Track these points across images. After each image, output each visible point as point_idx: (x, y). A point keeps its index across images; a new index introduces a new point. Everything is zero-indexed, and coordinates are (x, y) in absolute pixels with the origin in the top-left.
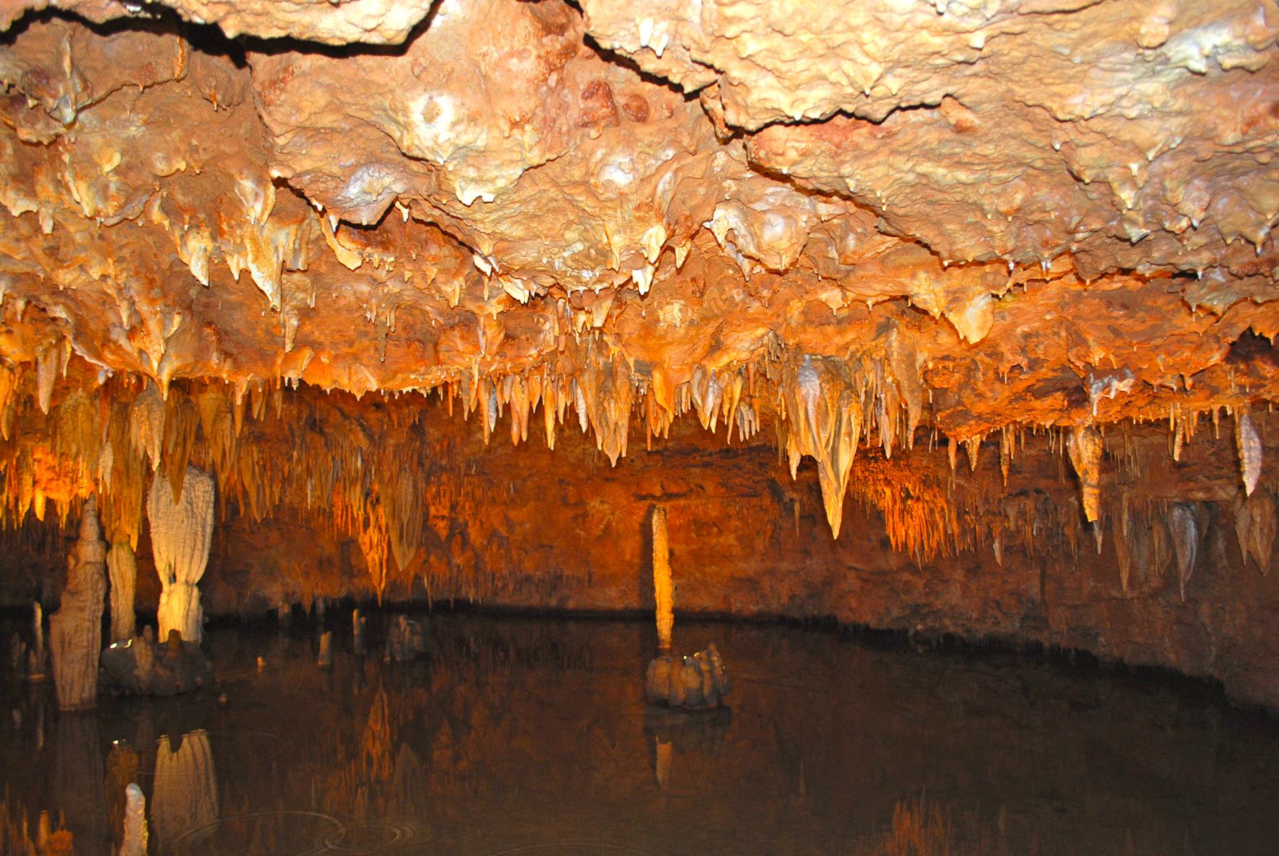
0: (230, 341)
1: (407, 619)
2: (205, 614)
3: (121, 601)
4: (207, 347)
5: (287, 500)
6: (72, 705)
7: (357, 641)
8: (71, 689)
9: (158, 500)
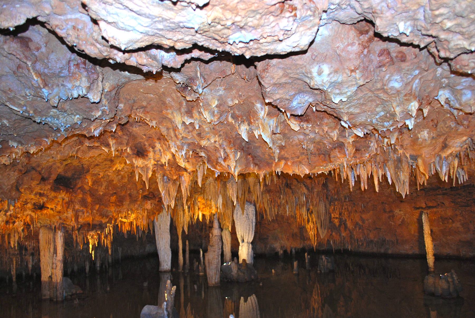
1: (325, 257)
2: (254, 253)
3: (227, 248)
4: (249, 163)
5: (280, 213)
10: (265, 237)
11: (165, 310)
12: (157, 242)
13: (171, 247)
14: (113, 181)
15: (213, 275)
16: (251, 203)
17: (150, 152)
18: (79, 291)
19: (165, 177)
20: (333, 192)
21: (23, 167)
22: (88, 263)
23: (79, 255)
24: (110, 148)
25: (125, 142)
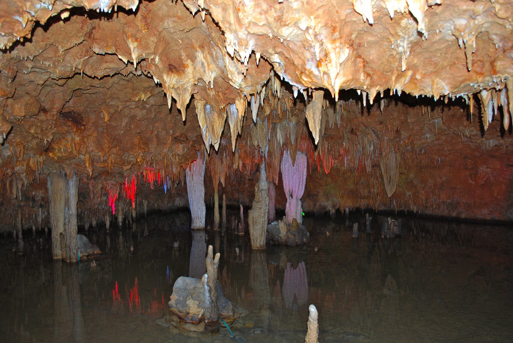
0: (369, 67)
1: (391, 219)
4: (359, 70)
6: (257, 247)
7: (368, 227)
8: (257, 241)
9: (285, 164)
10: (315, 193)
11: (206, 284)
12: (189, 196)
13: (205, 202)
14: (136, 117)
15: (258, 236)
16: (302, 152)
17: (187, 66)
18: (97, 251)
19: (208, 106)
20: (407, 141)
21: (7, 86)
22: (108, 218)
23: (98, 207)
24: (131, 54)
25: (152, 46)
